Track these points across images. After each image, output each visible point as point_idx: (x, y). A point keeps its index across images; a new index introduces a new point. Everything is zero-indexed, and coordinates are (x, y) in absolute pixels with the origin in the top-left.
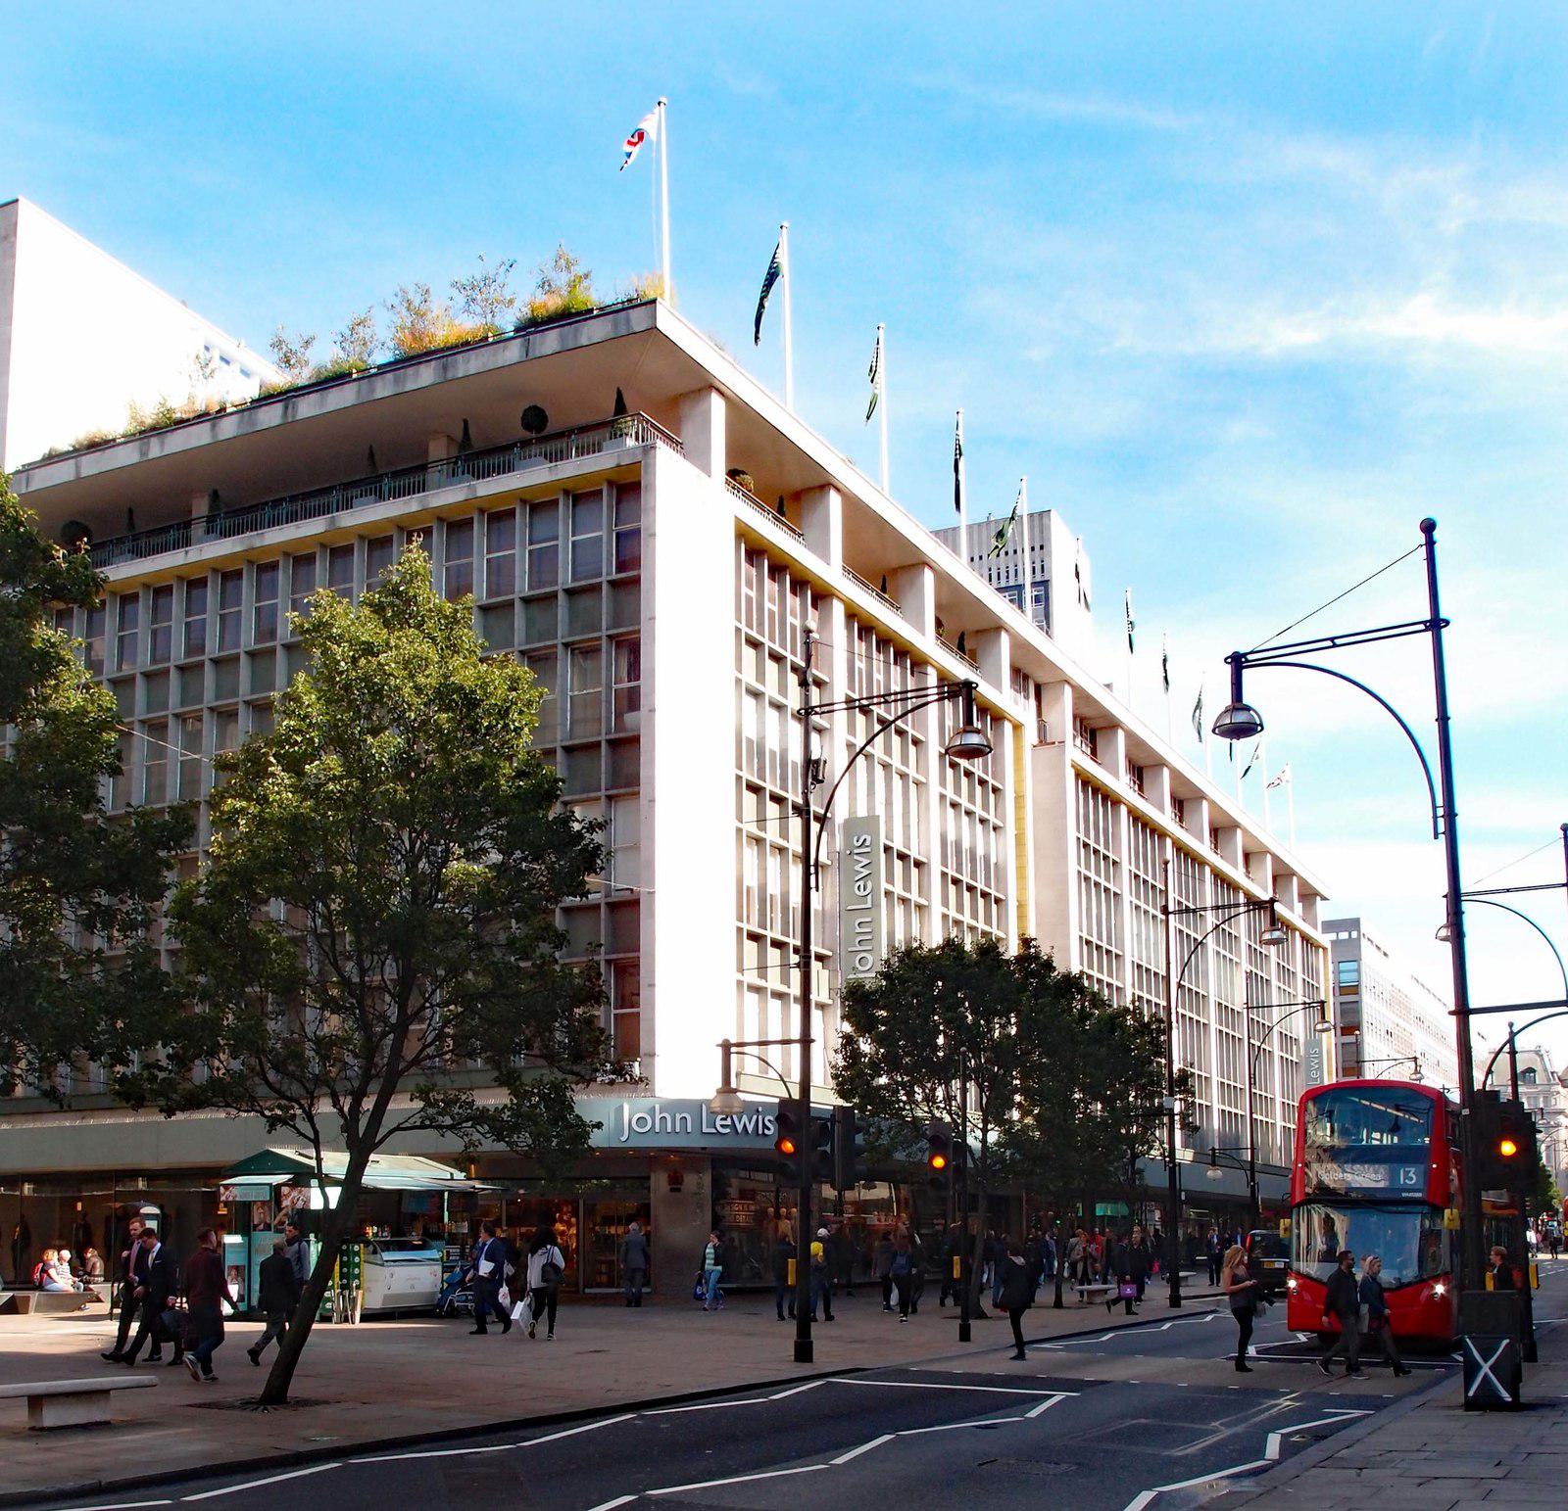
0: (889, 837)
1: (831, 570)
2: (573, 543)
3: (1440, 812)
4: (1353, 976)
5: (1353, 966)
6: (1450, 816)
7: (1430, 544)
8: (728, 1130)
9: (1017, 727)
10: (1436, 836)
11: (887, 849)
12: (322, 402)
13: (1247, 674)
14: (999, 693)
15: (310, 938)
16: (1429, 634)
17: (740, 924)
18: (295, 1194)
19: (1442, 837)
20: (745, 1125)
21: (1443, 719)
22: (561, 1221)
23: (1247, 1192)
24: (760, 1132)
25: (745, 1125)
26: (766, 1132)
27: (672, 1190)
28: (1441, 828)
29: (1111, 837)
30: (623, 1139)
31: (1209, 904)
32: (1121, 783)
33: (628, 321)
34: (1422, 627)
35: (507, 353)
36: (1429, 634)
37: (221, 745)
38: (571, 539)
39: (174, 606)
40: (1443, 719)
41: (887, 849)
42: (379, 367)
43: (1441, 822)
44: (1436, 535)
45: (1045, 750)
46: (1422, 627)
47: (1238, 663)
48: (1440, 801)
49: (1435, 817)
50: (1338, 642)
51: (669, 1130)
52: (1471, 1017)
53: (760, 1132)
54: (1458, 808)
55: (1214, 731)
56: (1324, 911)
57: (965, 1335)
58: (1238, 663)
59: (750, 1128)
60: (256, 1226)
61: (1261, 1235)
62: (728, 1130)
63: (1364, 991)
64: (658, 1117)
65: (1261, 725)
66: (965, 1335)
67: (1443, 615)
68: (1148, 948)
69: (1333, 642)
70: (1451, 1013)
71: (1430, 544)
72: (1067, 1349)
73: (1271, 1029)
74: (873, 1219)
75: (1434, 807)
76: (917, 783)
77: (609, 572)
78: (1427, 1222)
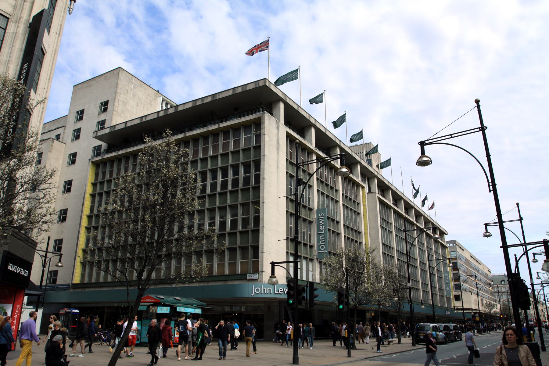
0: (329, 214)
1: (312, 145)
2: (244, 138)
3: (491, 184)
4: (455, 255)
5: (455, 253)
6: (494, 185)
7: (478, 106)
8: (282, 293)
9: (363, 187)
10: (490, 192)
11: (329, 218)
12: (184, 107)
13: (426, 147)
14: (357, 178)
16: (481, 132)
18: (153, 308)
19: (492, 192)
21: (488, 156)
22: (19, 306)
23: (431, 313)
27: (268, 310)
28: (491, 189)
29: (389, 216)
30: (252, 295)
32: (390, 203)
33: (259, 83)
34: (478, 130)
35: (229, 93)
36: (481, 132)
38: (244, 137)
40: (488, 156)
41: (329, 218)
43: (491, 187)
44: (480, 103)
45: (370, 195)
46: (478, 130)
47: (423, 144)
48: (490, 181)
49: (489, 186)
50: (453, 136)
51: (265, 292)
52: (509, 249)
54: (497, 182)
55: (416, 164)
56: (447, 238)
57: (349, 355)
58: (423, 144)
59: (323, 220)
60: (144, 318)
61: (329, 336)
62: (282, 293)
63: (458, 259)
65: (431, 161)
66: (349, 355)
67: (485, 125)
68: (400, 247)
69: (451, 136)
70: (501, 247)
71: (478, 106)
72: (381, 360)
73: (434, 268)
75: (489, 183)
77: (253, 144)
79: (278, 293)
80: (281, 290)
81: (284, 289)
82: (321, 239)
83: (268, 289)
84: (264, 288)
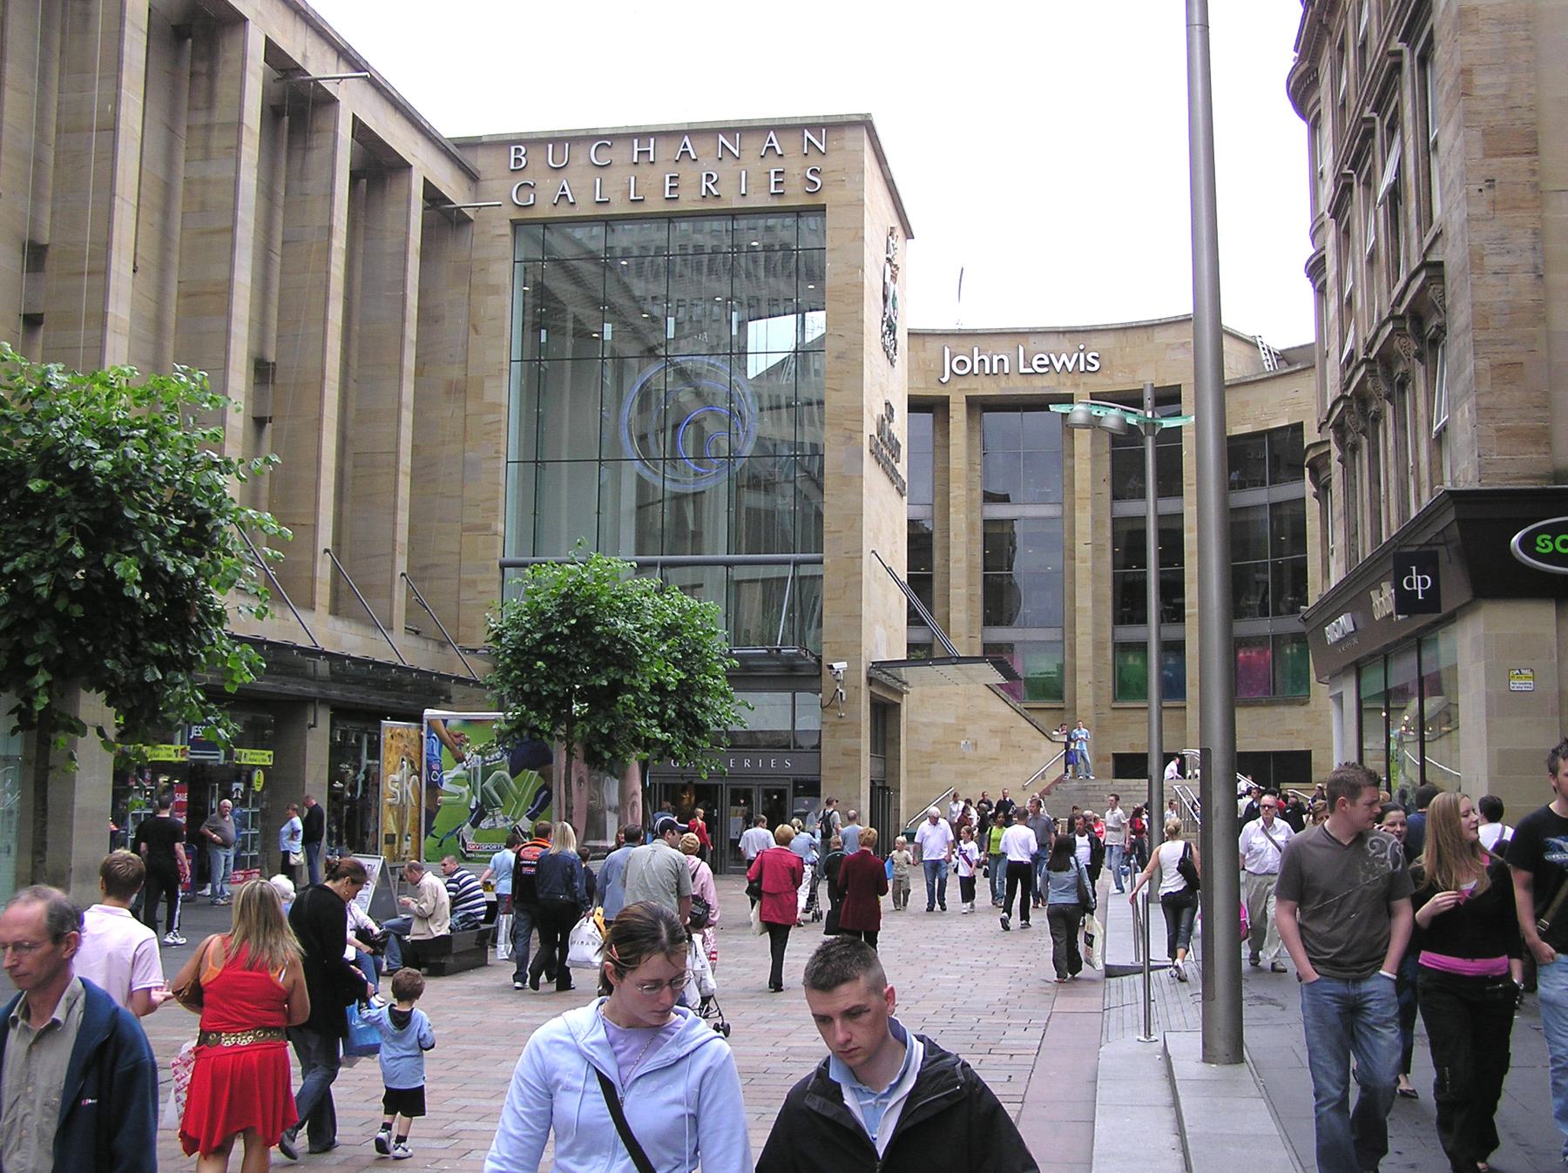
15: (1290, 624)
17: (1130, 508)
20: (1064, 363)
24: (1082, 369)
25: (1064, 363)
26: (1089, 368)
31: (784, 410)
37: (399, 969)
39: (308, 1000)
42: (1284, 357)
51: (987, 371)
53: (1082, 369)
59: (1070, 366)
62: (1045, 370)
64: (976, 359)
74: (657, 699)
76: (271, 947)
78: (483, 917)
79: (1030, 370)
80: (1042, 359)
81: (1052, 356)
82: (996, 359)
83: (996, 359)
84: (1001, 357)
